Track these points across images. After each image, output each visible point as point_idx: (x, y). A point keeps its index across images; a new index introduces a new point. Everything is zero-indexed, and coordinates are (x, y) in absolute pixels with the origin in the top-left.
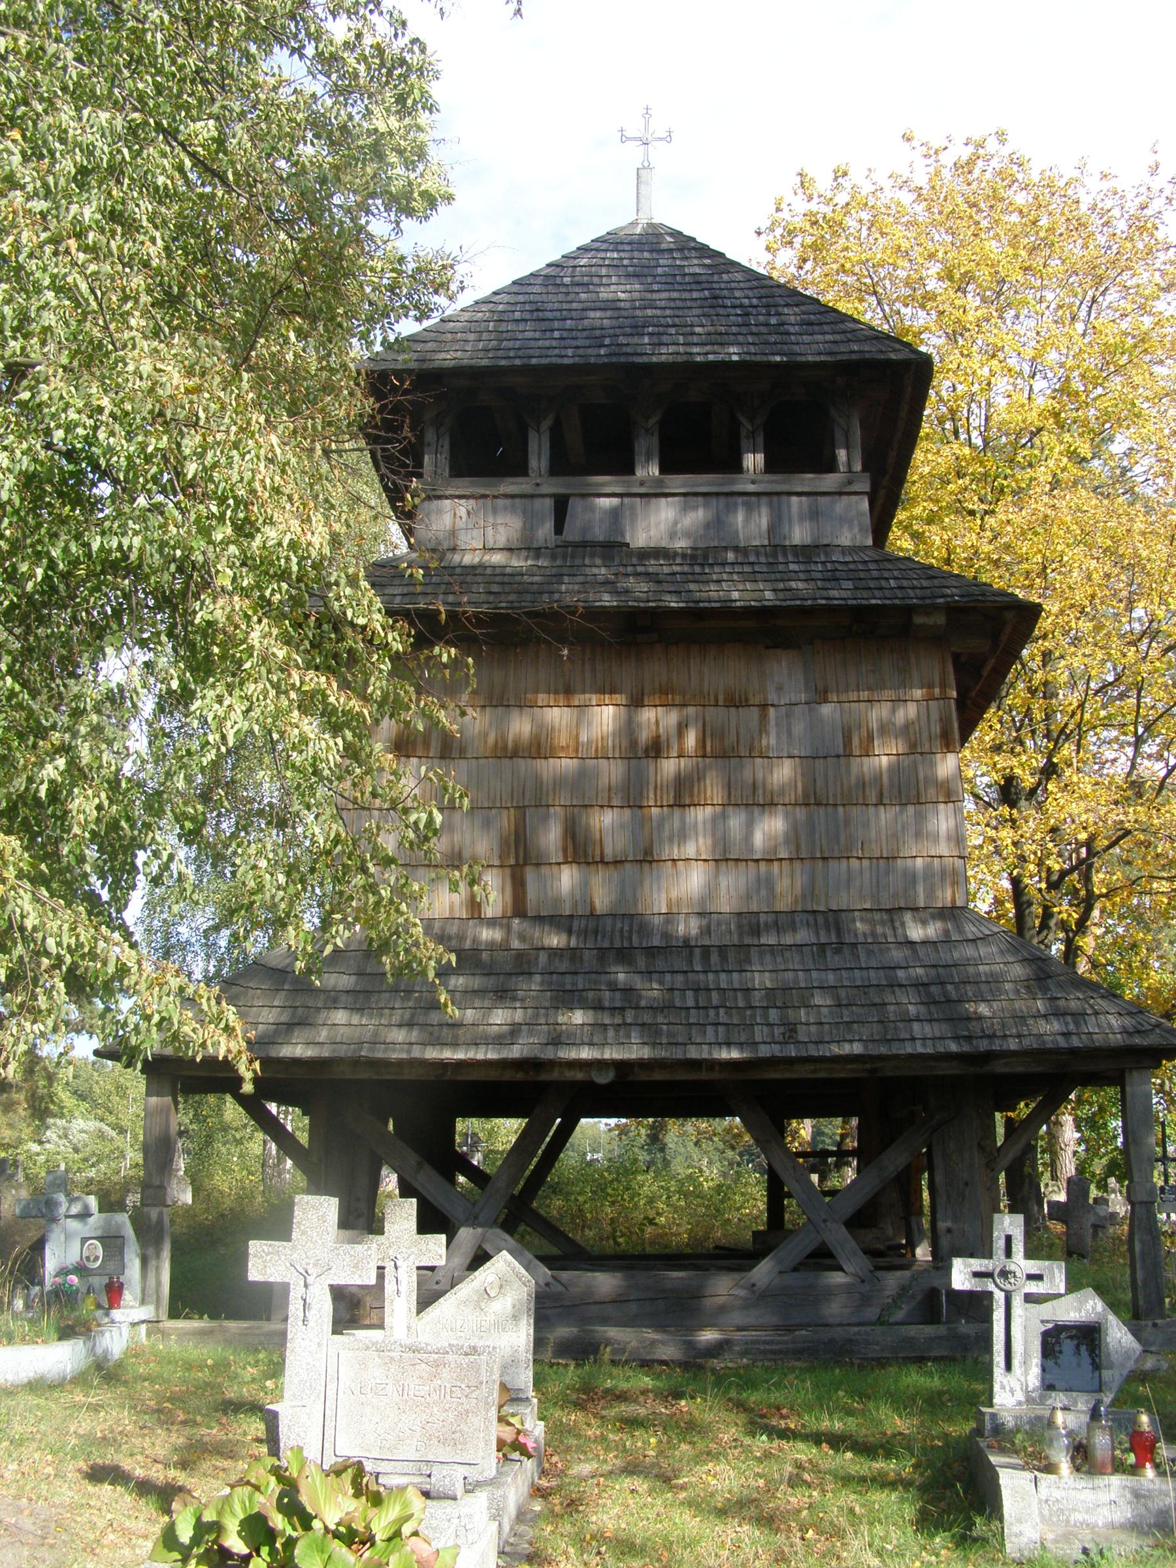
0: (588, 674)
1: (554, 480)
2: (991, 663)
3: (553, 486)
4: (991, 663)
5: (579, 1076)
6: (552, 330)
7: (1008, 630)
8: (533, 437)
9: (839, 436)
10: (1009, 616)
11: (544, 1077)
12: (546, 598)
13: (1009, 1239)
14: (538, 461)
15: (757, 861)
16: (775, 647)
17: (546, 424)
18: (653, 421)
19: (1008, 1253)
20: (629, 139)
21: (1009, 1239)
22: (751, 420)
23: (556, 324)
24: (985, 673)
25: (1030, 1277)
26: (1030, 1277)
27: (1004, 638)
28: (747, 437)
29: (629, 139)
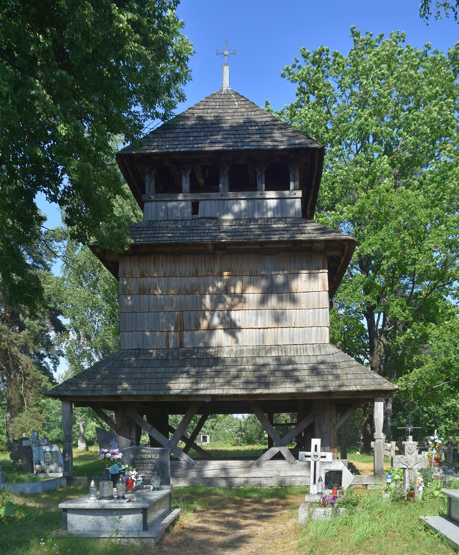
0: (203, 265)
1: (191, 194)
2: (343, 259)
3: (191, 197)
4: (343, 259)
5: (200, 399)
6: (189, 137)
7: (347, 248)
8: (183, 178)
9: (291, 176)
10: (346, 243)
11: (189, 400)
12: (187, 238)
13: (316, 446)
14: (186, 185)
15: (259, 328)
16: (267, 255)
17: (188, 173)
18: (225, 172)
19: (316, 450)
20: (219, 54)
21: (316, 446)
22: (260, 171)
23: (191, 134)
24: (342, 262)
25: (322, 457)
26: (322, 457)
27: (346, 250)
28: (259, 177)
29: (219, 54)
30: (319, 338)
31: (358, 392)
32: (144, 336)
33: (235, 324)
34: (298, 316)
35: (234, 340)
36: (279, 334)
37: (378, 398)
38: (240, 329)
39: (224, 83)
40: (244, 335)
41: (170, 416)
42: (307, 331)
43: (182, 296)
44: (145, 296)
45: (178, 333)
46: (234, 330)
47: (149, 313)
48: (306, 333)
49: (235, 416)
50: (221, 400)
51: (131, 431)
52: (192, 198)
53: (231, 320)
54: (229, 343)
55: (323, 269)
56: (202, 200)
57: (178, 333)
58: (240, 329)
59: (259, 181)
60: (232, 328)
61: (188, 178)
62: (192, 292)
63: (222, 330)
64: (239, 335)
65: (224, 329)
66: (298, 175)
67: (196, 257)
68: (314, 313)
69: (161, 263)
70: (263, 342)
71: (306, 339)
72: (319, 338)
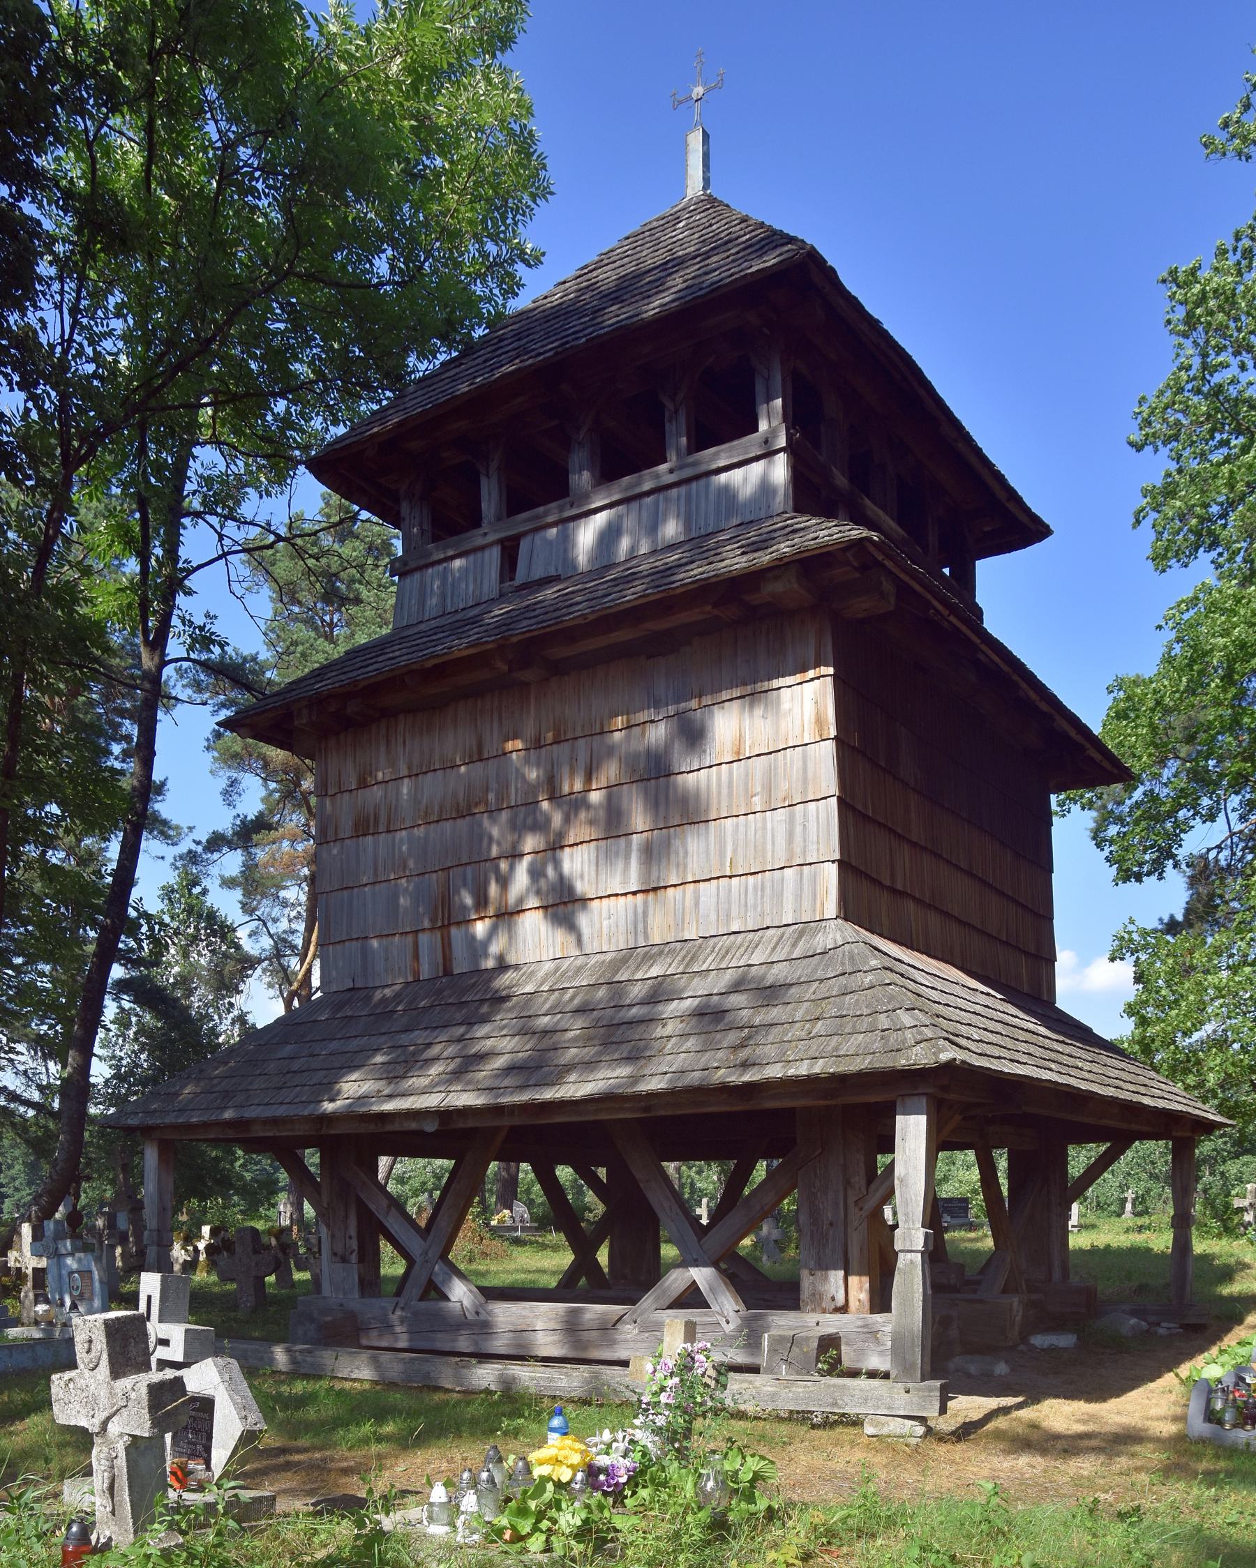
0: (496, 725)
11: (389, 1128)
15: (634, 893)
20: (680, 102)
28: (670, 422)
29: (680, 102)
30: (806, 904)
31: (811, 1080)
32: (365, 951)
33: (571, 889)
34: (741, 836)
35: (571, 939)
36: (689, 902)
37: (908, 1101)
38: (584, 901)
39: (689, 182)
40: (596, 917)
41: (879, 1157)
42: (768, 884)
43: (448, 825)
44: (370, 838)
45: (438, 934)
46: (570, 906)
47: (377, 887)
48: (768, 891)
49: (489, 1171)
50: (461, 1125)
51: (346, 1217)
52: (503, 535)
53: (561, 877)
54: (558, 948)
55: (817, 665)
56: (524, 534)
57: (438, 934)
58: (584, 901)
59: (670, 428)
60: (563, 904)
61: (494, 480)
62: (464, 811)
63: (540, 913)
64: (583, 920)
65: (545, 908)
66: (778, 378)
67: (479, 703)
68: (791, 820)
69: (400, 740)
70: (646, 936)
71: (768, 910)
72: (806, 904)
